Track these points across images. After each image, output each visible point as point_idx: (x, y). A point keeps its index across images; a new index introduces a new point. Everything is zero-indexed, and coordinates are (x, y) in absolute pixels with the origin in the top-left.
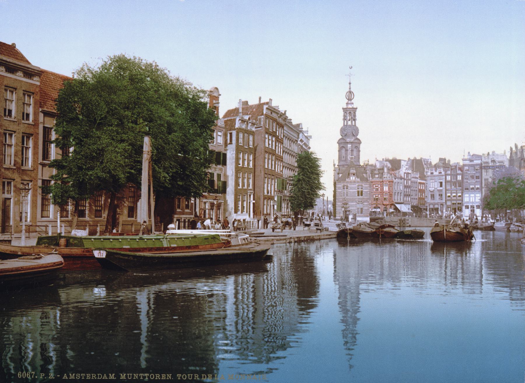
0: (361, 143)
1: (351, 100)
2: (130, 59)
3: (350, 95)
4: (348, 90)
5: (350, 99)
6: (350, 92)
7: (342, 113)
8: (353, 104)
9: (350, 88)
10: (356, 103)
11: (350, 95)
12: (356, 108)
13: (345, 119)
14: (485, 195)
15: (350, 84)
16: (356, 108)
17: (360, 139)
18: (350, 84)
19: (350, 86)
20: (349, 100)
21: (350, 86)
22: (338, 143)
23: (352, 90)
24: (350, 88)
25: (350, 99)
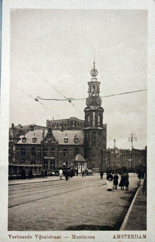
0: (103, 111)
1: (95, 76)
2: (144, 149)
3: (94, 73)
4: (93, 68)
5: (94, 75)
6: (94, 70)
7: (88, 87)
8: (97, 79)
9: (94, 67)
10: (99, 78)
11: (94, 73)
12: (146, 238)
13: (90, 92)
14: (16, 128)
15: (94, 63)
16: (146, 238)
17: (103, 108)
18: (94, 63)
19: (94, 65)
20: (93, 76)
21: (94, 65)
23: (96, 68)
24: (94, 67)
25: (94, 75)
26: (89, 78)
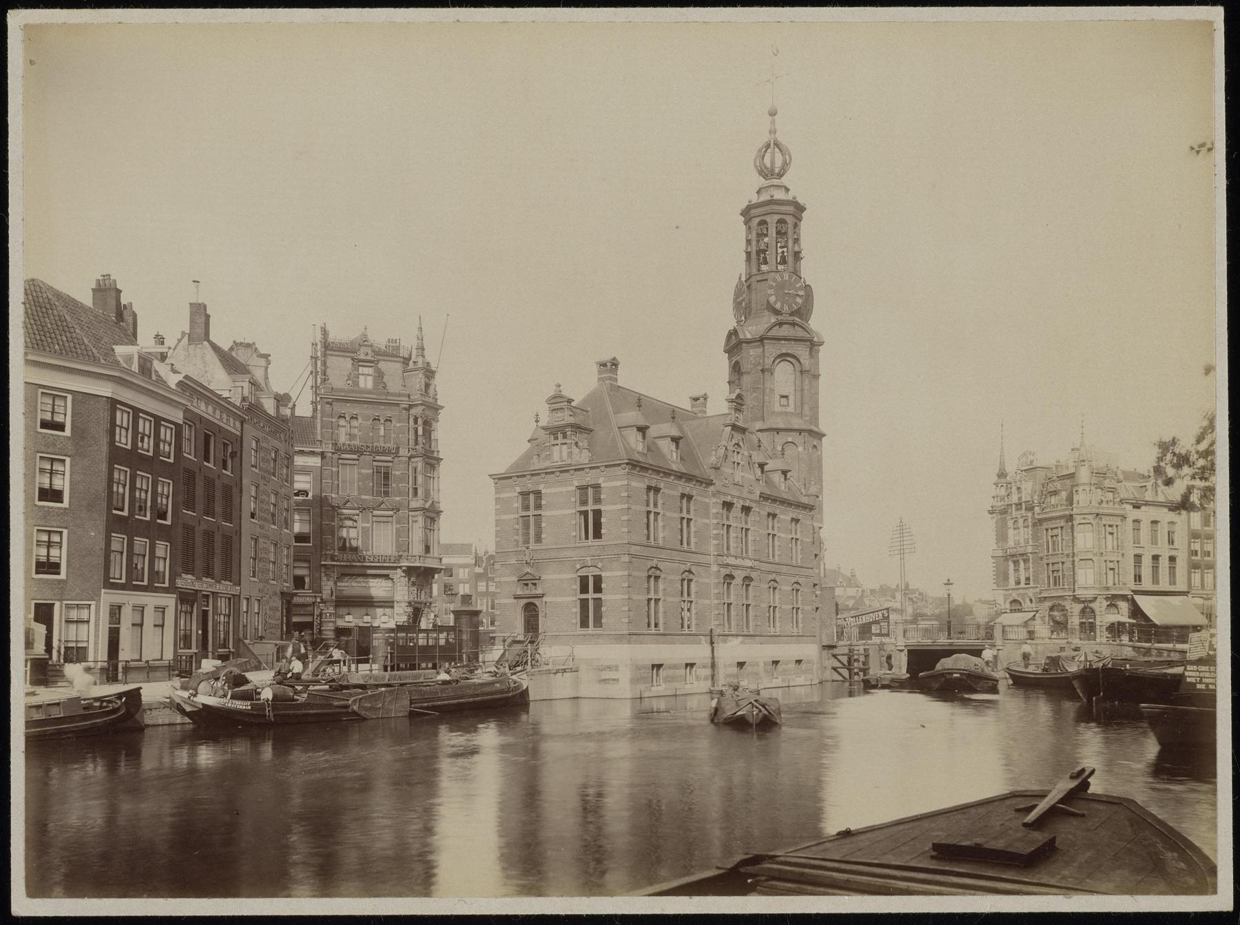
9: (773, 132)
10: (797, 185)
15: (773, 114)
18: (773, 114)
21: (773, 122)
22: (725, 352)
24: (773, 132)
26: (749, 188)
